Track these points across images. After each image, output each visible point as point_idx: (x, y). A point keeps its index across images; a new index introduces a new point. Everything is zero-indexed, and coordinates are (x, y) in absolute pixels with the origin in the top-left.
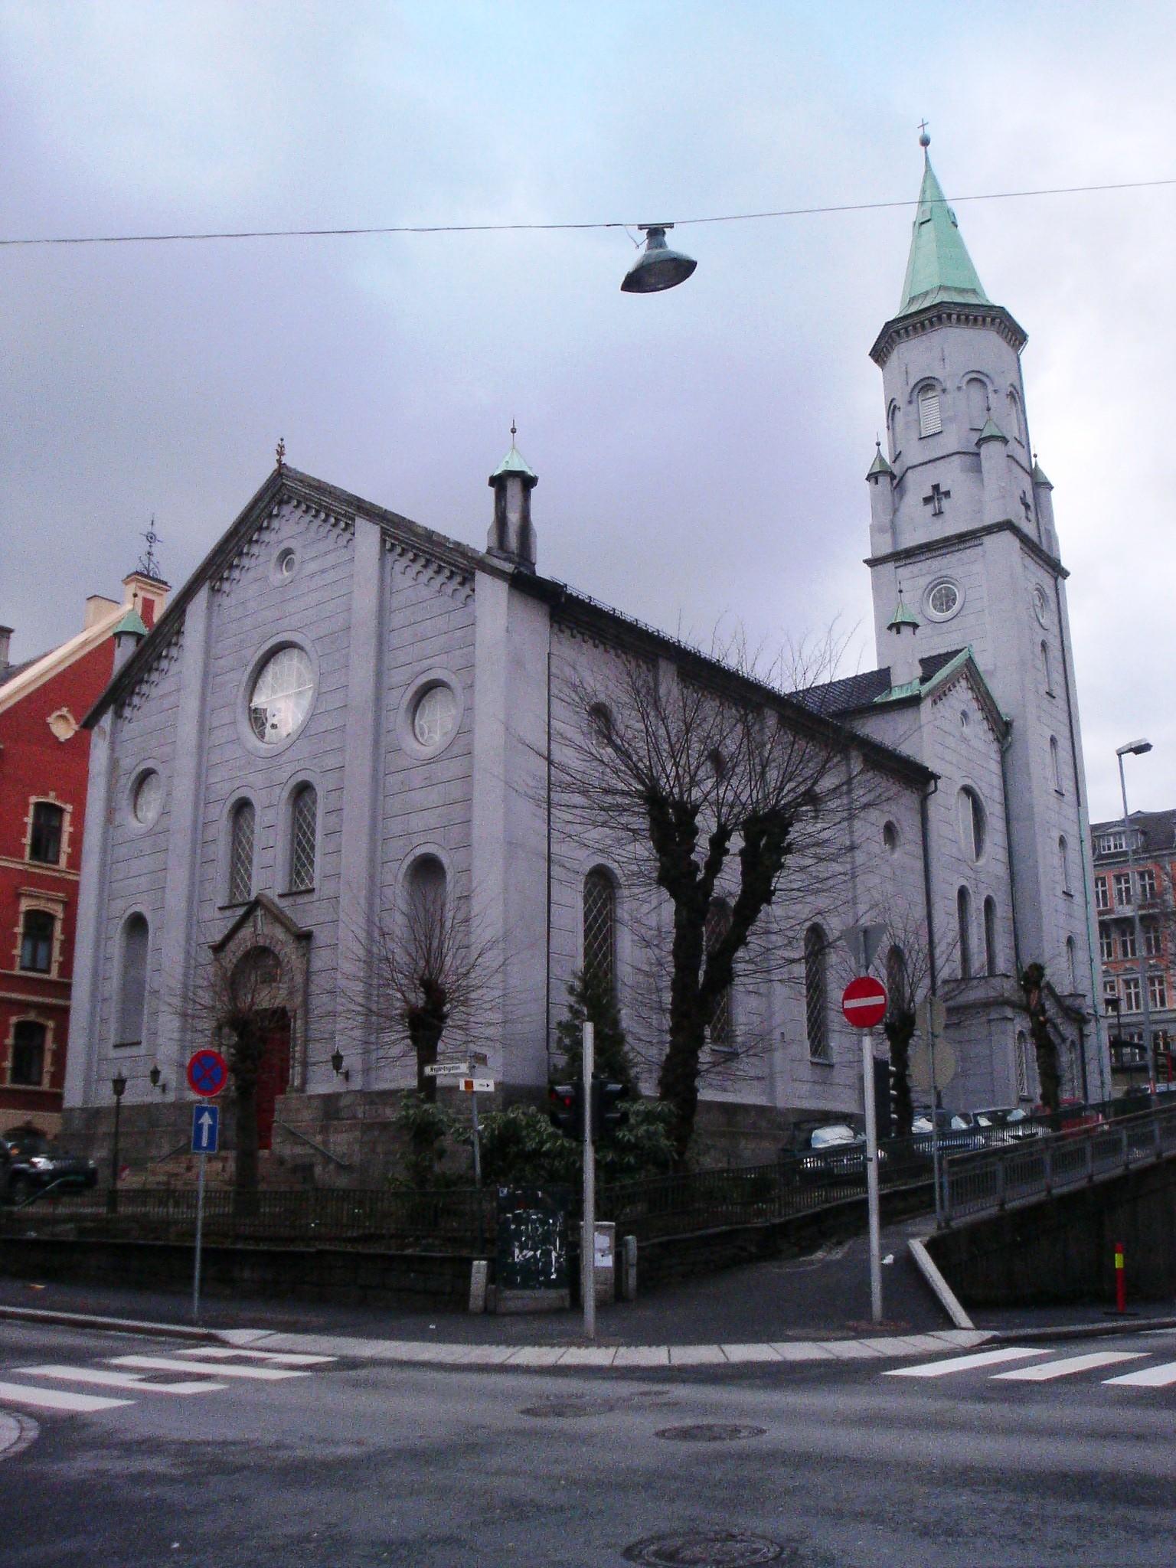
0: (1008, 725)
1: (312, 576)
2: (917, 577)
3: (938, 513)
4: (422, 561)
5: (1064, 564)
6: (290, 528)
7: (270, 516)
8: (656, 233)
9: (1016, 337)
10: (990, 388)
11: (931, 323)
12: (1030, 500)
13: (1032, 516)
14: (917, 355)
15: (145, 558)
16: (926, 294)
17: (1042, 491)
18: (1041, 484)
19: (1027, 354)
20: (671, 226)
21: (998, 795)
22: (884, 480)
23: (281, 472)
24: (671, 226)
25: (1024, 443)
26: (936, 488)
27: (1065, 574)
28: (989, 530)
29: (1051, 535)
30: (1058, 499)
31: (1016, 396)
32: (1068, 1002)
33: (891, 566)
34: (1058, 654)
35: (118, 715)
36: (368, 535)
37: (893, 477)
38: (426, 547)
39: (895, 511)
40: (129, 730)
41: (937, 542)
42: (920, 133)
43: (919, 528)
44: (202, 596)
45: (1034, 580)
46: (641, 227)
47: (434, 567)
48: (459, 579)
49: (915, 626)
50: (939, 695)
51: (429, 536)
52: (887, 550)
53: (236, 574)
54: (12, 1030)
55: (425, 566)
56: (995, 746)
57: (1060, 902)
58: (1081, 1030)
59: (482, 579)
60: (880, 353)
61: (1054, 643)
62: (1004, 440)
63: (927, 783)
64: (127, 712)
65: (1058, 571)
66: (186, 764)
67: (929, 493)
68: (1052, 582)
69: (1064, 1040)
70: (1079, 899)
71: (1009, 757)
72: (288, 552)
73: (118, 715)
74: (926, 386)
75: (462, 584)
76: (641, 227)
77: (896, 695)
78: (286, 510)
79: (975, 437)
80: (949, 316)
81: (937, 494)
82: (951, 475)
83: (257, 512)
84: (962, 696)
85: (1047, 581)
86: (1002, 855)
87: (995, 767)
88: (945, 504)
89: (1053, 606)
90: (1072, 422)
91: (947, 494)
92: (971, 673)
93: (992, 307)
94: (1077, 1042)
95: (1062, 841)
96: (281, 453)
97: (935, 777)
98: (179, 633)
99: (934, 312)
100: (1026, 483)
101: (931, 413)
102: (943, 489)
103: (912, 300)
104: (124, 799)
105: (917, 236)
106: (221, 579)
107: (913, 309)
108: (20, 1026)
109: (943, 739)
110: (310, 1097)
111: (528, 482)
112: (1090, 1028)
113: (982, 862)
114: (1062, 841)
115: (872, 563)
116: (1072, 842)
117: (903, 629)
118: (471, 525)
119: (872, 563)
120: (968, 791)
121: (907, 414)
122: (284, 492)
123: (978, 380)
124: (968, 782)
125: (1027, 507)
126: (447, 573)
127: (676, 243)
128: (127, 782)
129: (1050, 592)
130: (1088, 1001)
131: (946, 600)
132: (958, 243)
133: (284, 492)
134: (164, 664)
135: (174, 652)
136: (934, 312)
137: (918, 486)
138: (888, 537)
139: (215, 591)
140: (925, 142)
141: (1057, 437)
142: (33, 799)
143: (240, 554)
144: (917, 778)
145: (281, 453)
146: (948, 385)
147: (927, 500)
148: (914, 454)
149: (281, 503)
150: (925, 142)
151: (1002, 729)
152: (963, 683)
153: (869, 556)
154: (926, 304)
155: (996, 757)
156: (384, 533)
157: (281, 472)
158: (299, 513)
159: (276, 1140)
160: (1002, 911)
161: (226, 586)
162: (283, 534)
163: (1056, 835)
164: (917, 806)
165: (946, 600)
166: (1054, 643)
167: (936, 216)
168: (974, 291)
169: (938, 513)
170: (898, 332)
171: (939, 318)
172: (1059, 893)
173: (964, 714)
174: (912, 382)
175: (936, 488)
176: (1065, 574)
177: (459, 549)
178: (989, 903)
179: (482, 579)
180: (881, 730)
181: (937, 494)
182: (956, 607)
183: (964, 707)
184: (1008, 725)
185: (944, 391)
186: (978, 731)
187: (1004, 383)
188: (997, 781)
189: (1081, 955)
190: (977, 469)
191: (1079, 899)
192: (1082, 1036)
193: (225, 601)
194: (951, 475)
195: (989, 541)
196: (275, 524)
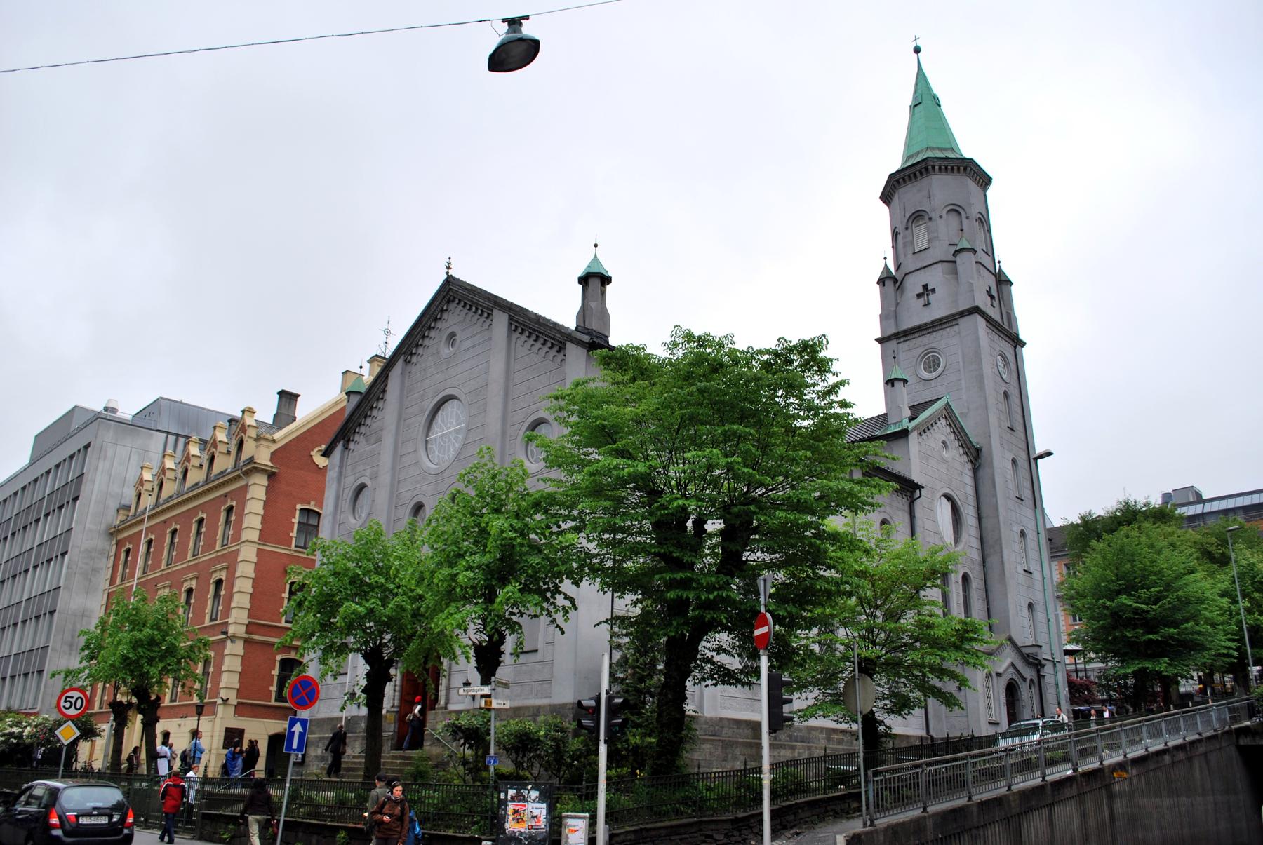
0: (978, 451)
1: (466, 350)
2: (911, 350)
3: (927, 304)
4: (534, 337)
5: (1022, 337)
6: (454, 319)
7: (442, 311)
8: (514, 23)
9: (984, 180)
10: (964, 215)
11: (921, 173)
12: (994, 293)
13: (996, 303)
14: (911, 196)
15: (383, 345)
16: (918, 153)
17: (1004, 287)
18: (1002, 281)
19: (991, 193)
20: (527, 18)
21: (972, 500)
22: (889, 283)
23: (450, 282)
24: (527, 18)
25: (990, 252)
26: (925, 287)
27: (1023, 344)
28: (962, 314)
29: (1010, 317)
30: (1015, 290)
31: (984, 221)
32: (1025, 651)
33: (894, 342)
34: (1018, 401)
35: (346, 448)
36: (500, 319)
37: (895, 280)
38: (536, 326)
39: (897, 304)
40: (351, 458)
41: (926, 324)
42: (914, 45)
43: (916, 315)
44: (400, 364)
45: (998, 349)
46: (504, 21)
47: (541, 341)
48: (556, 348)
49: (905, 381)
50: (924, 430)
51: (538, 319)
52: (892, 331)
53: (420, 350)
54: (277, 664)
55: (543, 344)
56: (969, 466)
57: (1022, 577)
58: (1038, 672)
59: (570, 347)
60: (886, 197)
61: (1014, 393)
62: (975, 252)
63: (913, 492)
64: (351, 446)
65: (1017, 342)
66: (385, 478)
67: (920, 290)
68: (1012, 350)
69: (1024, 679)
70: (1037, 575)
71: (981, 473)
72: (453, 335)
73: (346, 448)
74: (917, 216)
75: (558, 351)
76: (504, 21)
77: (891, 430)
78: (452, 306)
79: (953, 249)
80: (933, 167)
81: (927, 290)
82: (935, 277)
83: (434, 307)
84: (942, 431)
85: (1008, 349)
86: (975, 543)
87: (968, 480)
88: (932, 297)
89: (1013, 366)
90: (1022, 233)
91: (933, 290)
92: (949, 414)
93: (964, 159)
94: (1036, 680)
95: (1022, 533)
96: (449, 268)
97: (919, 487)
98: (384, 391)
99: (923, 165)
100: (992, 282)
101: (921, 237)
102: (930, 287)
103: (908, 158)
104: (346, 505)
105: (912, 115)
106: (411, 354)
107: (909, 164)
108: (283, 661)
109: (930, 460)
110: (451, 712)
111: (605, 280)
112: (1048, 670)
113: (960, 548)
114: (1022, 533)
115: (879, 340)
116: (1031, 535)
117: (896, 383)
118: (562, 308)
119: (879, 340)
120: (948, 497)
121: (904, 237)
122: (455, 297)
123: (956, 210)
124: (947, 491)
125: (992, 297)
126: (549, 344)
127: (527, 30)
128: (348, 494)
129: (1011, 357)
130: (1045, 648)
131: (933, 364)
132: (940, 118)
133: (455, 297)
134: (375, 413)
135: (381, 404)
136: (923, 165)
137: (913, 285)
138: (892, 321)
139: (407, 362)
140: (917, 50)
141: (1012, 248)
142: (299, 507)
143: (424, 337)
144: (909, 489)
145: (449, 268)
146: (932, 215)
147: (919, 296)
148: (910, 265)
149: (448, 302)
150: (917, 50)
151: (975, 456)
152: (943, 421)
153: (879, 336)
154: (918, 159)
155: (971, 474)
156: (511, 318)
157: (450, 282)
158: (460, 308)
159: (427, 744)
160: (976, 584)
161: (414, 359)
162: (450, 322)
163: (1017, 529)
164: (906, 508)
165: (933, 364)
166: (1014, 393)
167: (925, 102)
168: (952, 150)
169: (927, 304)
170: (898, 181)
171: (927, 169)
172: (1020, 570)
173: (944, 443)
174: (908, 215)
175: (925, 287)
176: (1023, 344)
177: (556, 327)
178: (965, 578)
179: (570, 347)
180: (885, 457)
181: (927, 290)
182: (940, 369)
183: (943, 438)
184: (978, 451)
185: (930, 219)
186: (955, 455)
187: (974, 212)
188: (970, 490)
189: (1040, 616)
190: (955, 272)
191: (1037, 575)
192: (1040, 677)
193: (414, 369)
194: (935, 277)
195: (964, 322)
196: (445, 316)
